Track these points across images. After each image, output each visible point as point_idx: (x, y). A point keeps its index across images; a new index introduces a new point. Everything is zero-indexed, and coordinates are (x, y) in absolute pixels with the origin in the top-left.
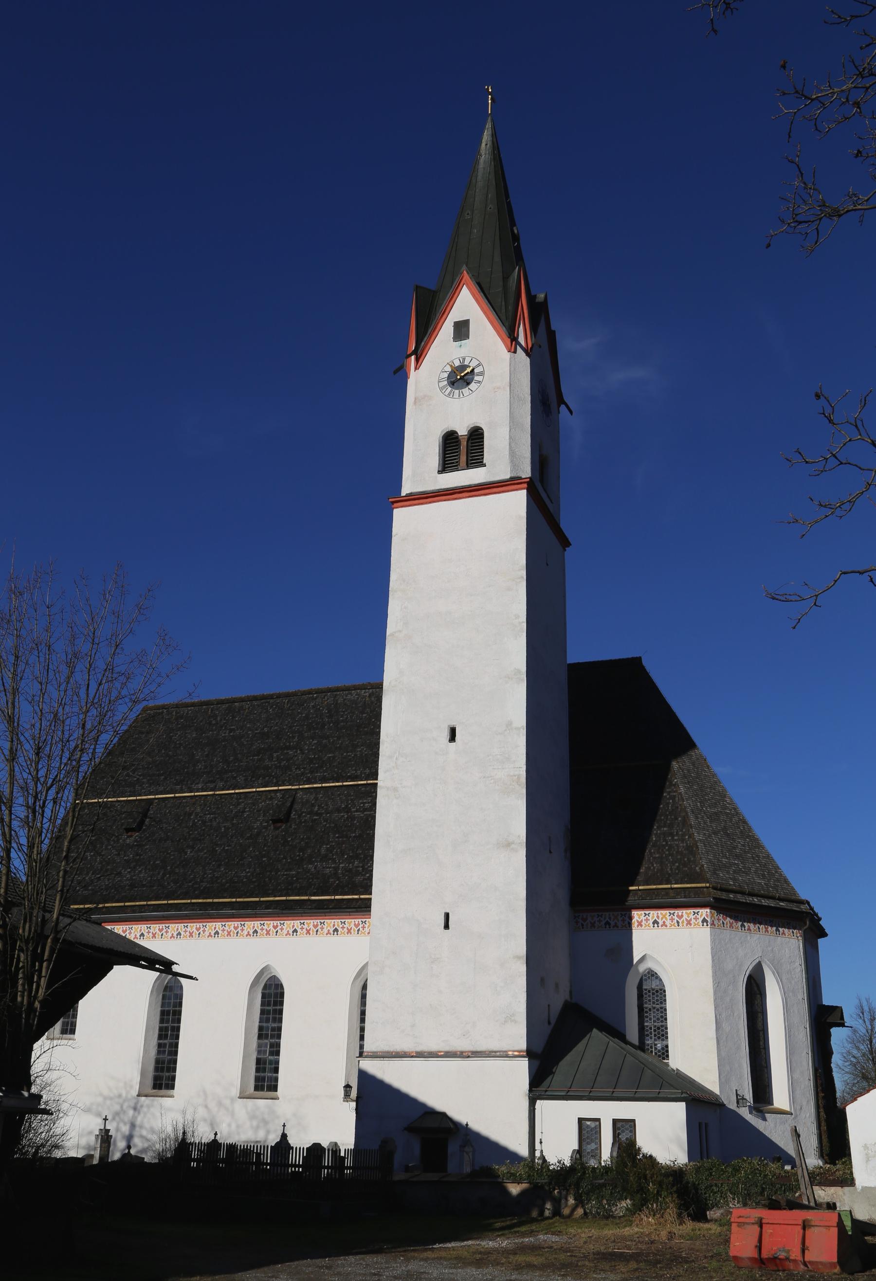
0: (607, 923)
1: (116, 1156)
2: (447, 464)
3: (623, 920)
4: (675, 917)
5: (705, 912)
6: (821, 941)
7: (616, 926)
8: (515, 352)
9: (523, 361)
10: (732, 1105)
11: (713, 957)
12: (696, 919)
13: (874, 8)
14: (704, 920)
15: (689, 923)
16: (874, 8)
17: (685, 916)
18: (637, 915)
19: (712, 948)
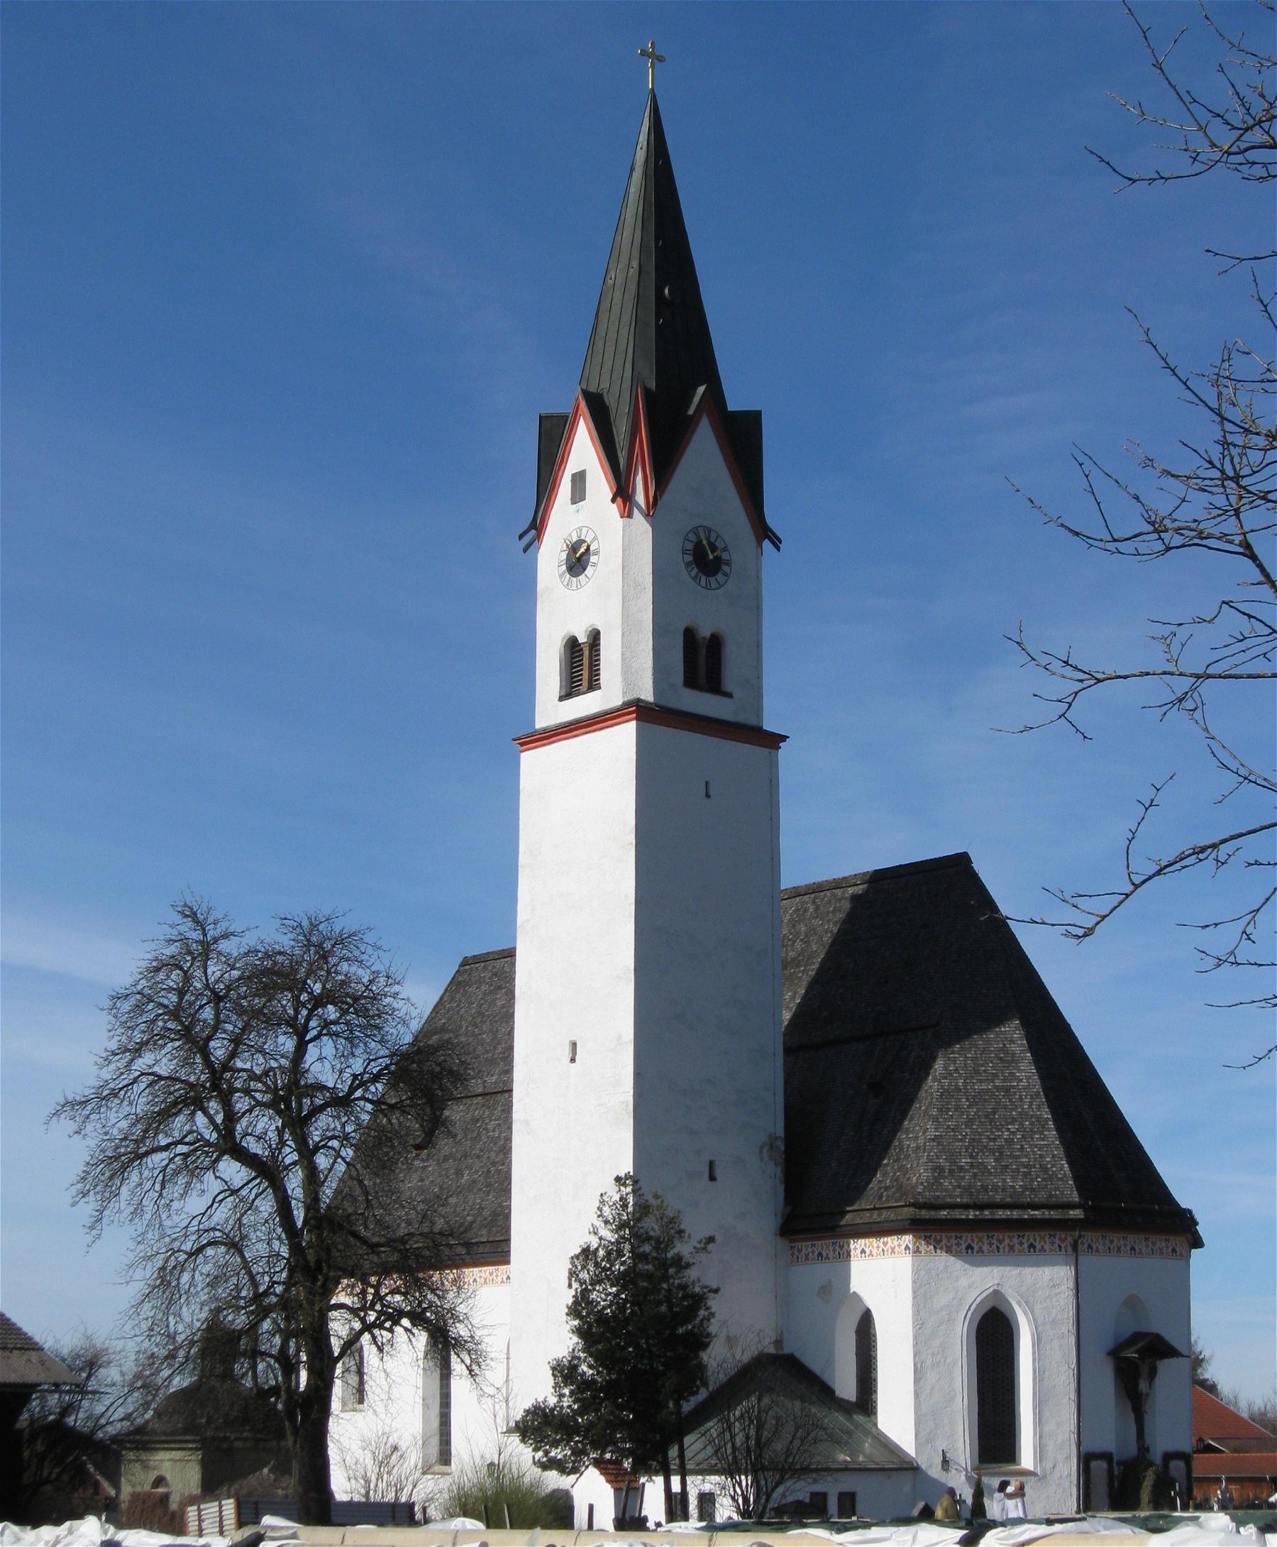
0: (1031, 1246)
1: (403, 1500)
2: (569, 692)
3: (834, 1251)
4: (1057, 1241)
5: (907, 1239)
6: (1195, 1253)
7: (1043, 1249)
8: (630, 516)
9: (641, 527)
10: (935, 1472)
11: (914, 1292)
12: (1021, 1244)
13: (1274, 631)
14: (907, 1248)
15: (1011, 1248)
16: (1274, 631)
17: (890, 1243)
18: (856, 1245)
19: (914, 1282)
